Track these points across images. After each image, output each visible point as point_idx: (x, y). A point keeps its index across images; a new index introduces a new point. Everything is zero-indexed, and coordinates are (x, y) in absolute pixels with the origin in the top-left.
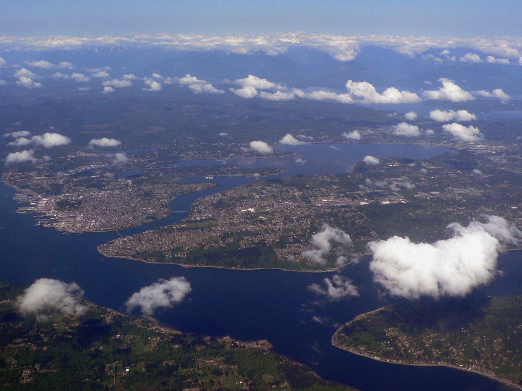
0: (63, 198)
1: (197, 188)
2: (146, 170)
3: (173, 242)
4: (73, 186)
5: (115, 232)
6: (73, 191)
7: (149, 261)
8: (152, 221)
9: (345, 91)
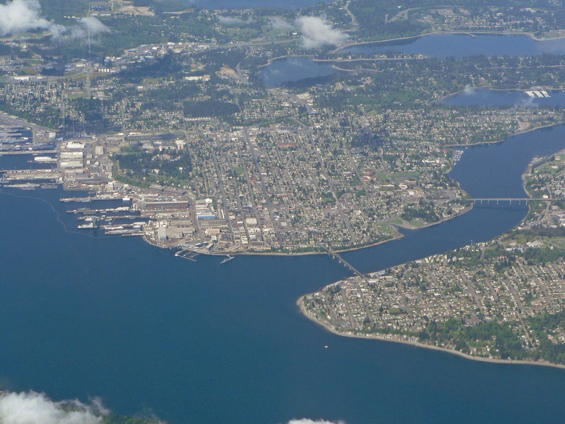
0: (124, 144)
1: (514, 124)
2: (337, 64)
3: (529, 298)
4: (144, 107)
5: (327, 258)
6: (149, 123)
7: (472, 355)
8: (426, 224)
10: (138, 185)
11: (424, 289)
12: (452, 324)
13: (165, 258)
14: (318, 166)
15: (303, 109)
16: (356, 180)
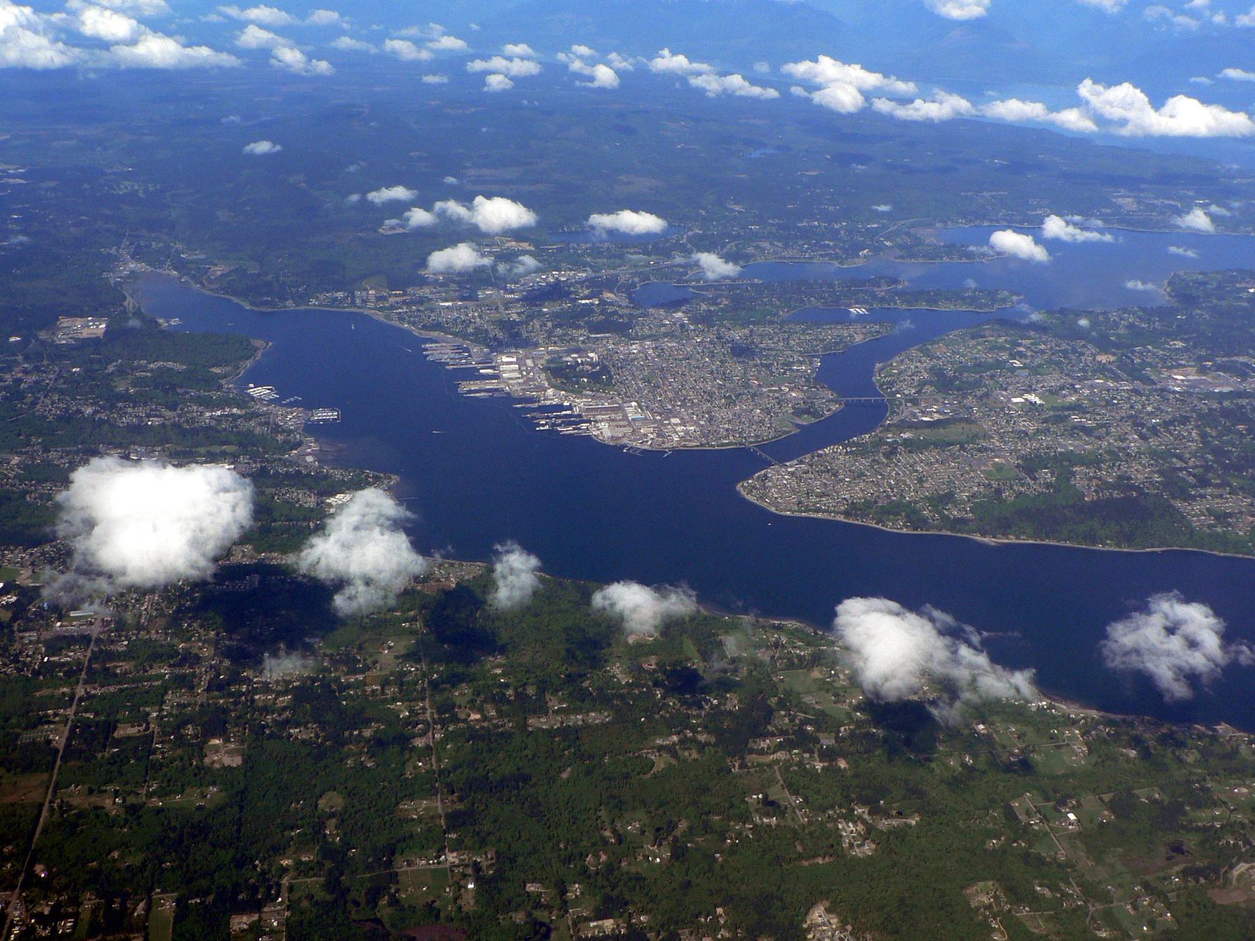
3: (920, 481)
4: (555, 326)
7: (889, 527)
8: (813, 420)
9: (1077, 102)
10: (572, 391)
11: (835, 475)
12: (868, 505)
13: (613, 452)
14: (712, 373)
15: (683, 326)
16: (746, 385)
